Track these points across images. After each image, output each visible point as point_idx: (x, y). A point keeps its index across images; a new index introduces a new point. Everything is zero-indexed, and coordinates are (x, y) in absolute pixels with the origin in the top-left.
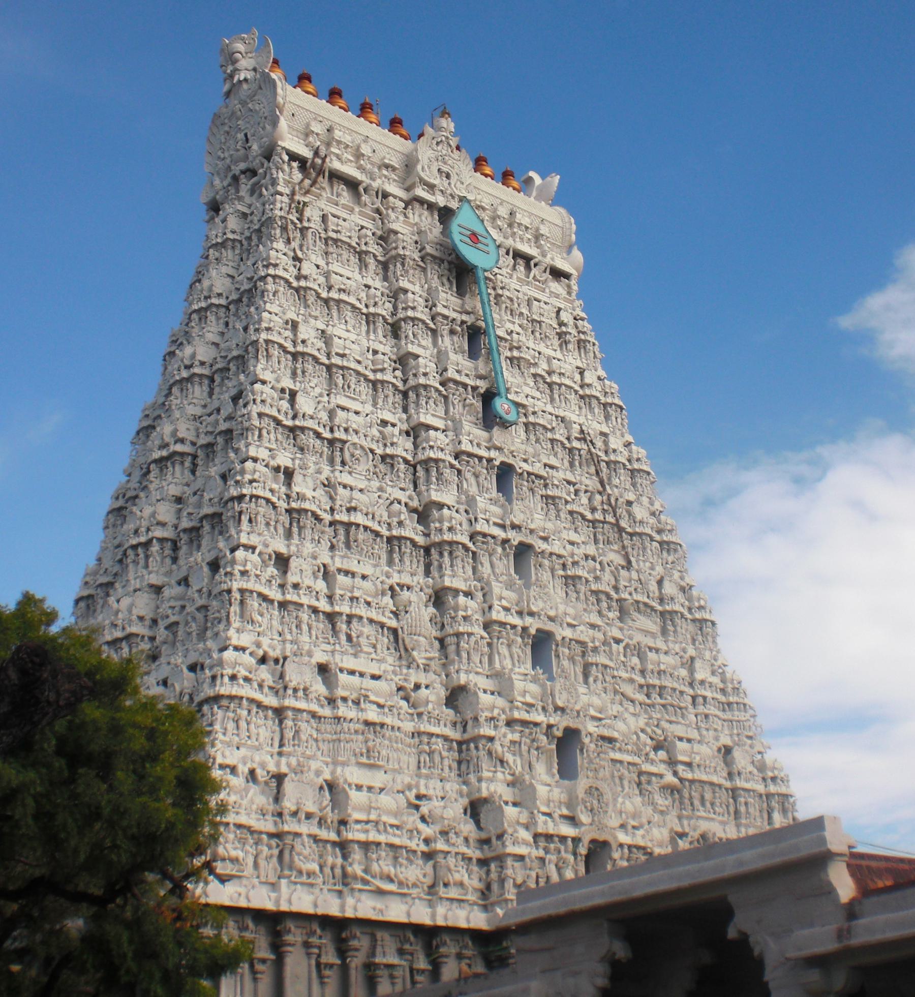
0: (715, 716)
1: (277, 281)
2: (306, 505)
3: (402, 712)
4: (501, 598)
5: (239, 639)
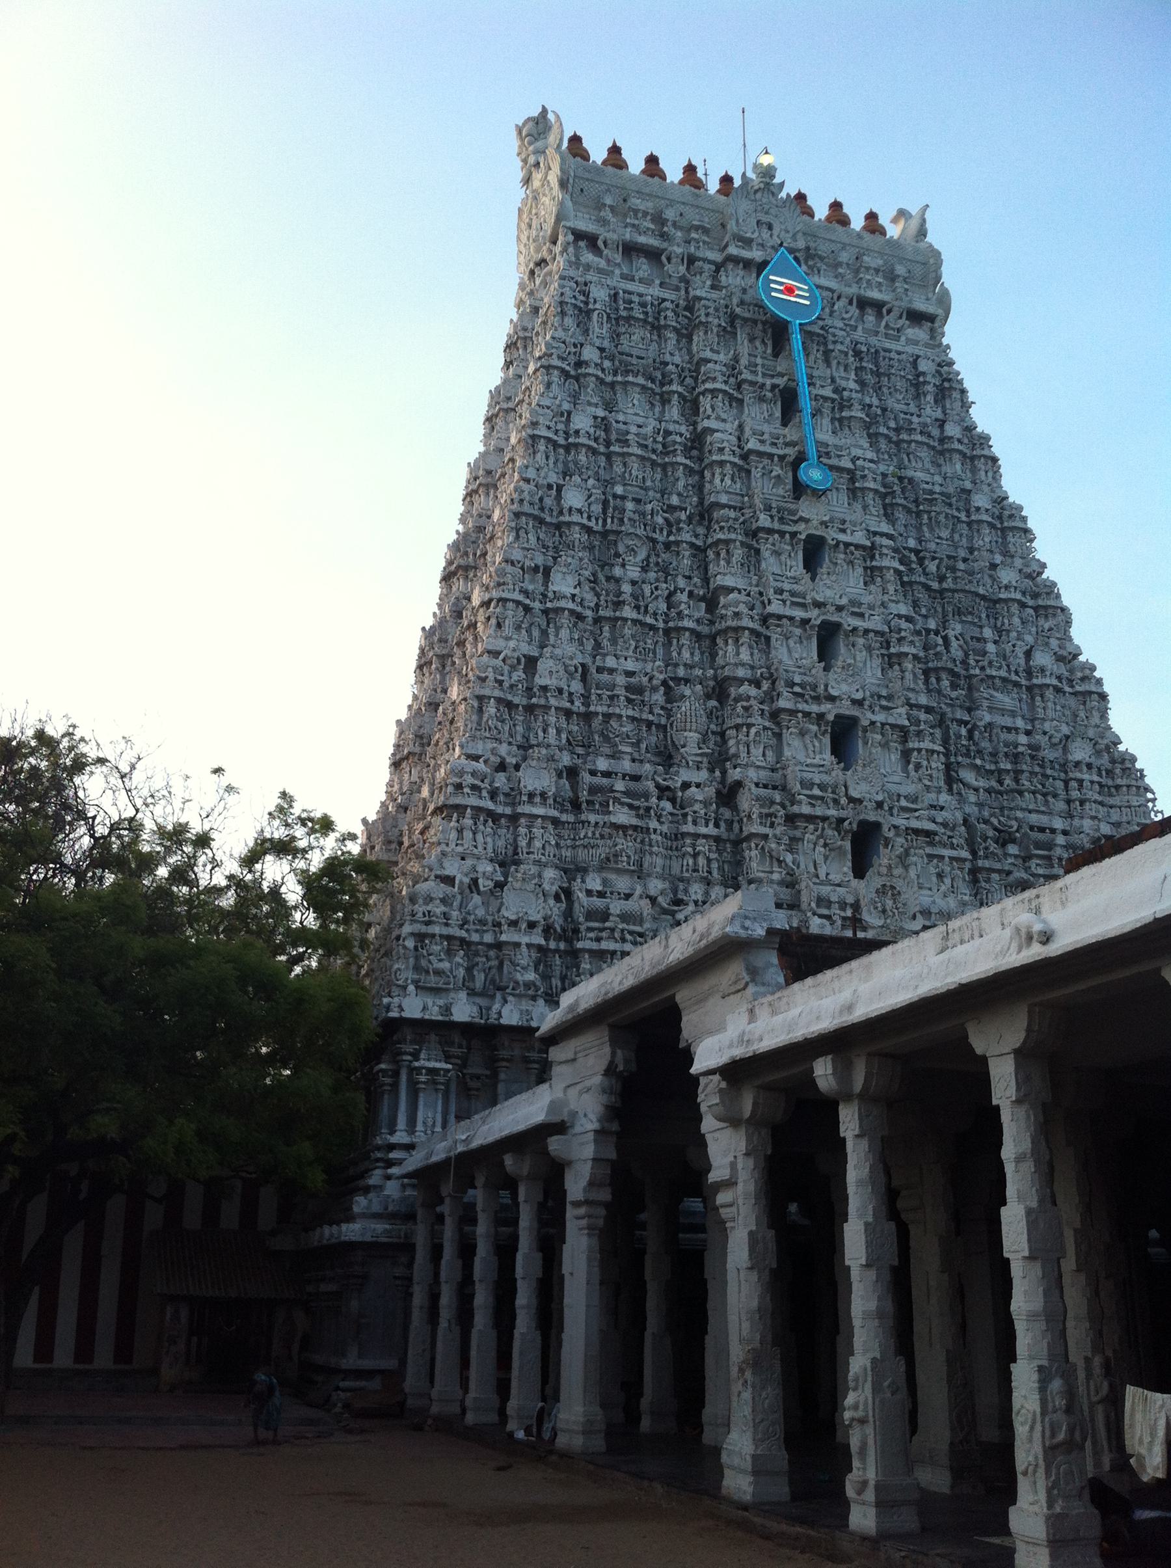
2: (562, 604)
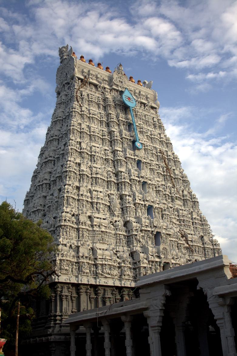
2: (84, 173)
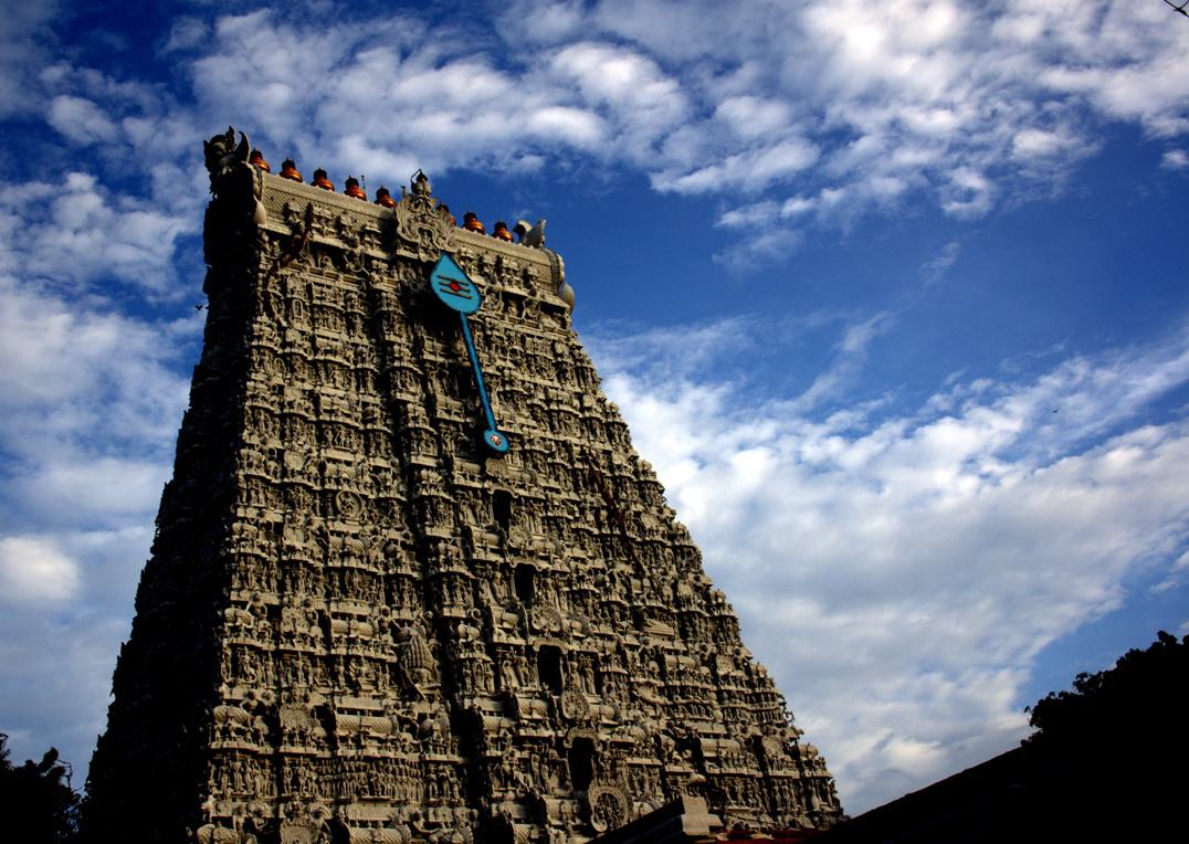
0: (742, 708)
1: (262, 351)
3: (407, 744)
4: (502, 621)
5: (231, 693)
